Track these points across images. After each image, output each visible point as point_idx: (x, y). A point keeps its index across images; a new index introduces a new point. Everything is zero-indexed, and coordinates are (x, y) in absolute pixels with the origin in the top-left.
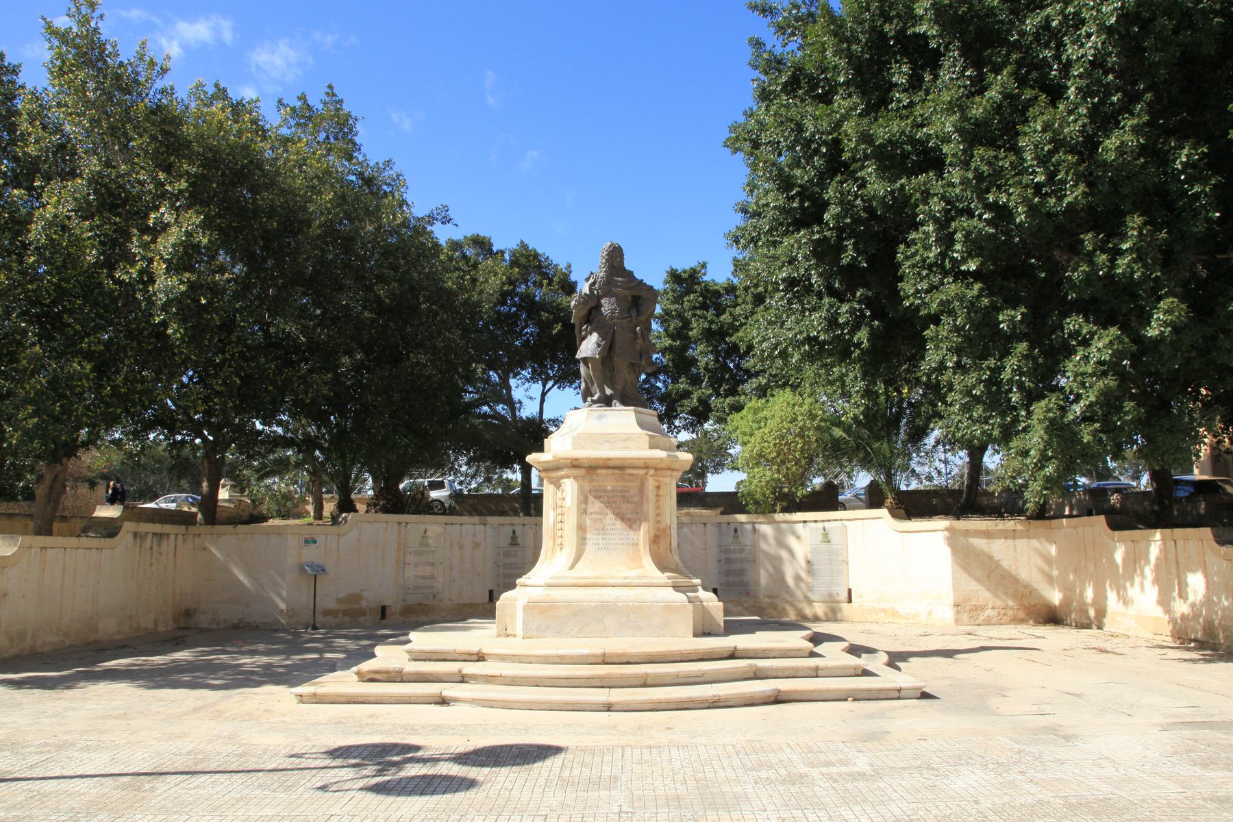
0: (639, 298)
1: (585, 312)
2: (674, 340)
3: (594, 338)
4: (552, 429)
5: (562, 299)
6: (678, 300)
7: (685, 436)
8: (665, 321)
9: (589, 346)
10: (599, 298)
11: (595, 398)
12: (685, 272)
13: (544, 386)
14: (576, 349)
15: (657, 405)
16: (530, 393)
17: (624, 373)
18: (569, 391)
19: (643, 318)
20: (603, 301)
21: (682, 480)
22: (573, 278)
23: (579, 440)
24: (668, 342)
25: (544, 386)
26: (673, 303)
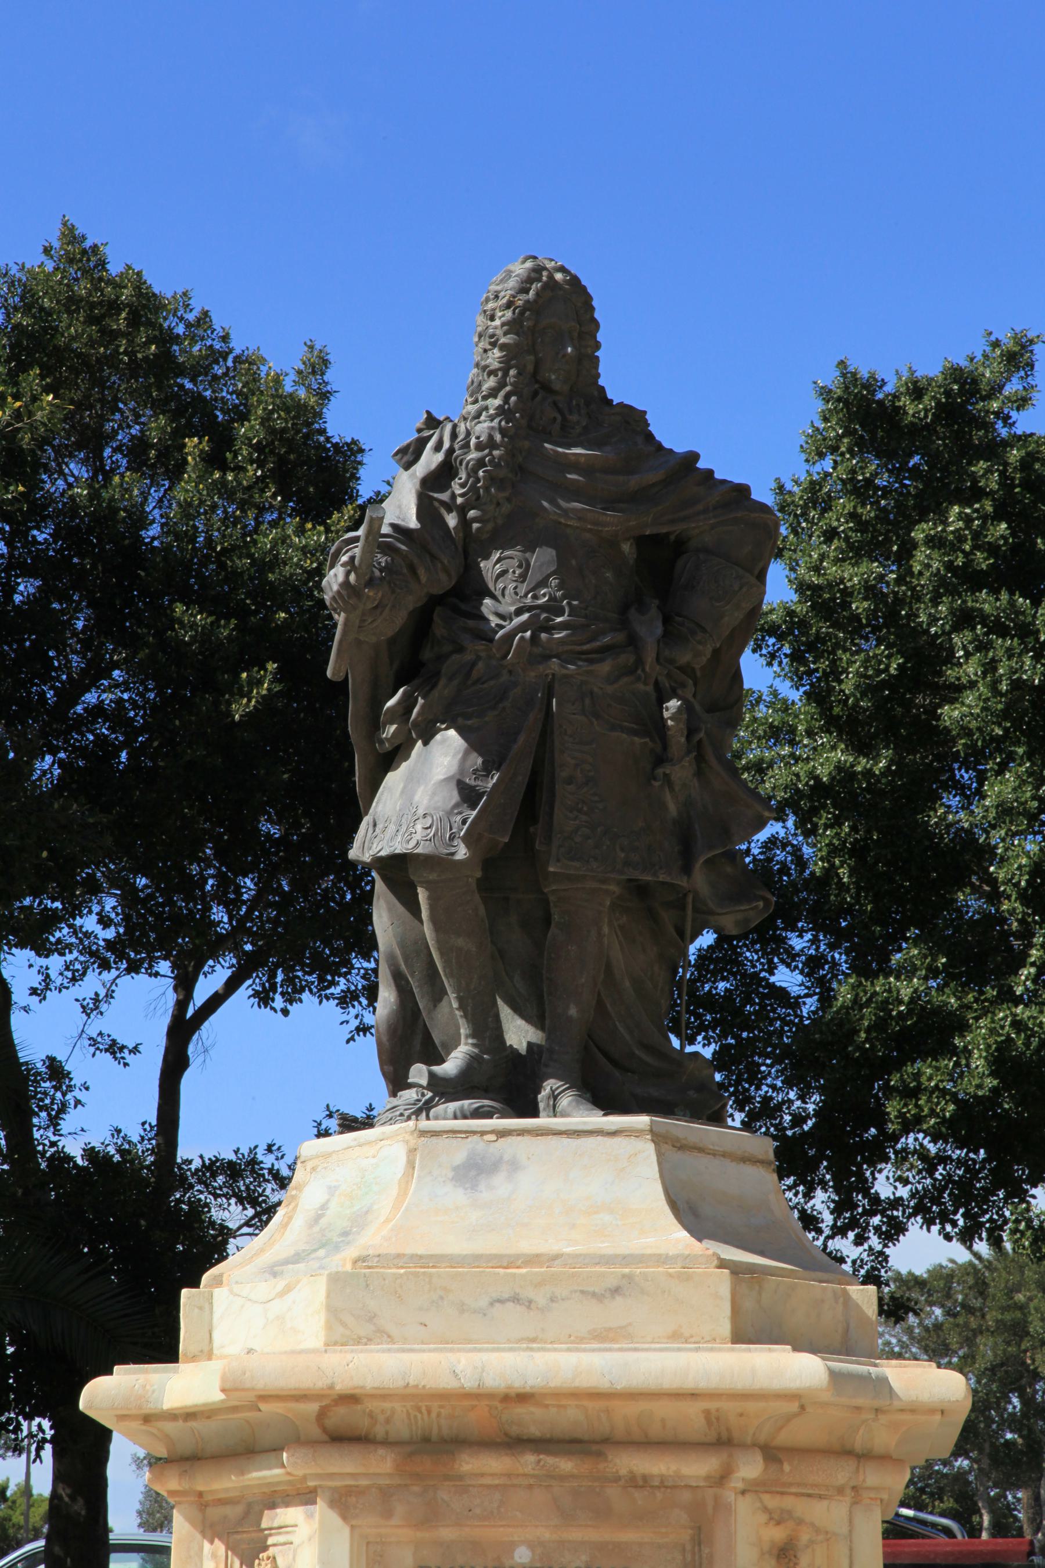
0: (679, 546)
1: (392, 622)
2: (862, 747)
3: (444, 754)
4: (231, 1214)
5: (284, 538)
6: (880, 536)
7: (923, 1250)
8: (815, 646)
9: (418, 799)
10: (470, 548)
11: (451, 1066)
12: (917, 391)
13: (185, 984)
14: (349, 812)
15: (774, 1085)
16: (112, 1022)
17: (600, 941)
18: (317, 1016)
19: (695, 654)
20: (489, 567)
21: (924, 1489)
22: (338, 424)
23: (367, 1292)
24: (830, 758)
25: (185, 984)
26: (856, 552)
